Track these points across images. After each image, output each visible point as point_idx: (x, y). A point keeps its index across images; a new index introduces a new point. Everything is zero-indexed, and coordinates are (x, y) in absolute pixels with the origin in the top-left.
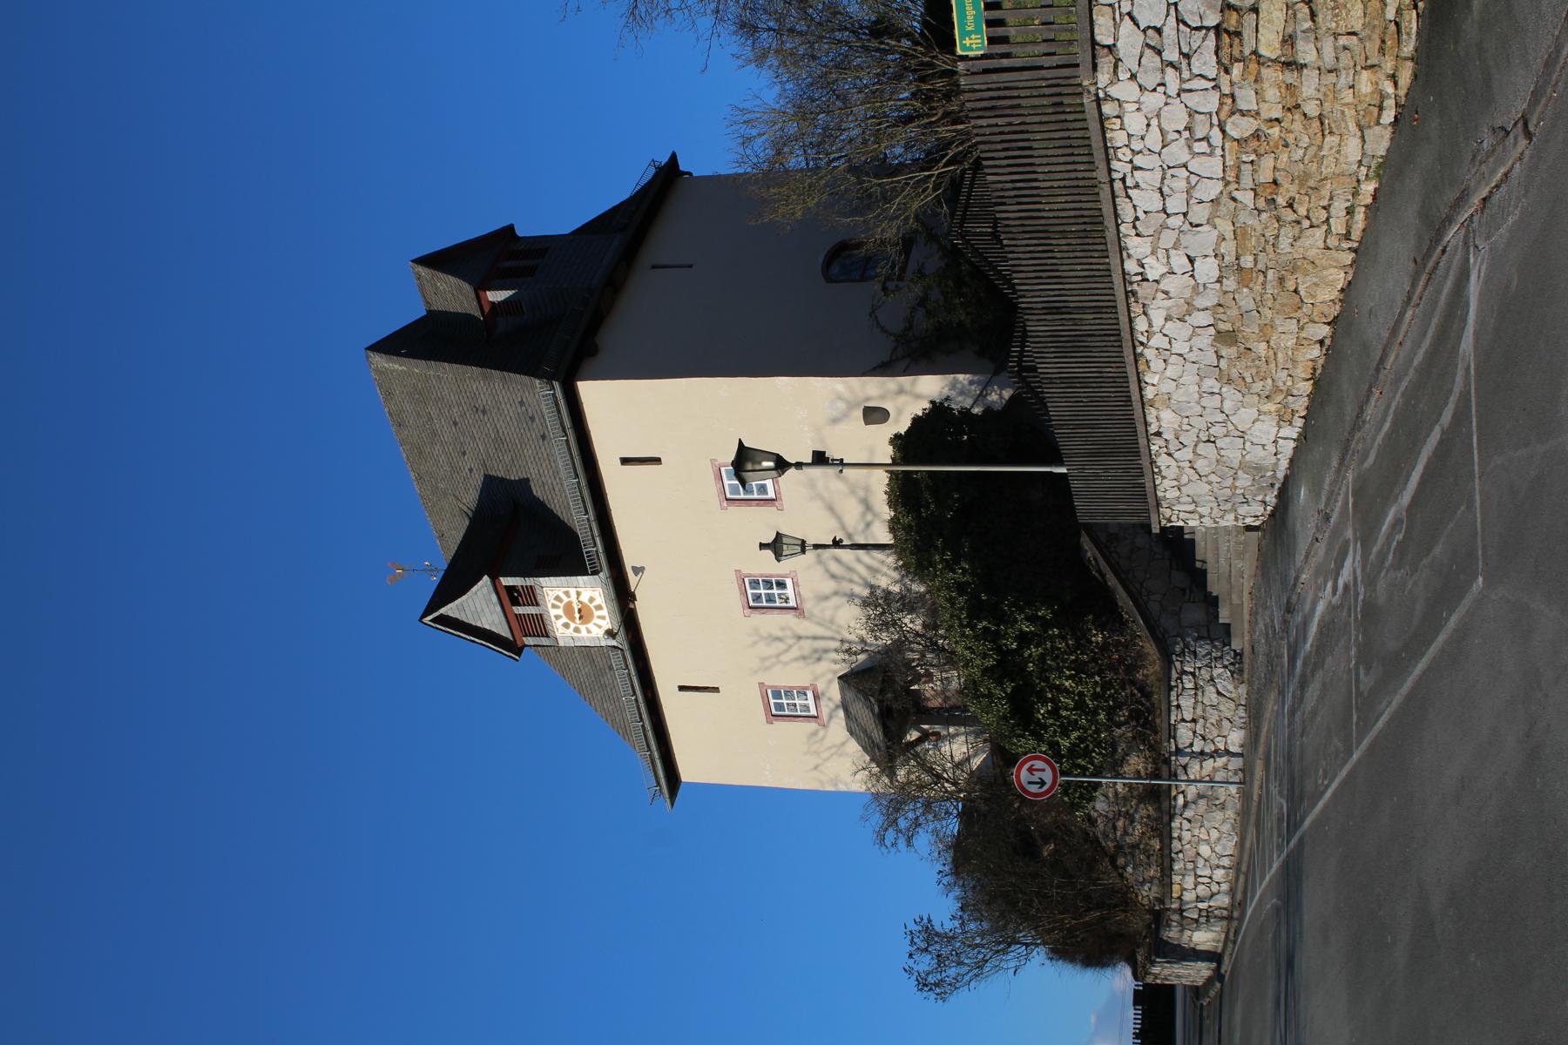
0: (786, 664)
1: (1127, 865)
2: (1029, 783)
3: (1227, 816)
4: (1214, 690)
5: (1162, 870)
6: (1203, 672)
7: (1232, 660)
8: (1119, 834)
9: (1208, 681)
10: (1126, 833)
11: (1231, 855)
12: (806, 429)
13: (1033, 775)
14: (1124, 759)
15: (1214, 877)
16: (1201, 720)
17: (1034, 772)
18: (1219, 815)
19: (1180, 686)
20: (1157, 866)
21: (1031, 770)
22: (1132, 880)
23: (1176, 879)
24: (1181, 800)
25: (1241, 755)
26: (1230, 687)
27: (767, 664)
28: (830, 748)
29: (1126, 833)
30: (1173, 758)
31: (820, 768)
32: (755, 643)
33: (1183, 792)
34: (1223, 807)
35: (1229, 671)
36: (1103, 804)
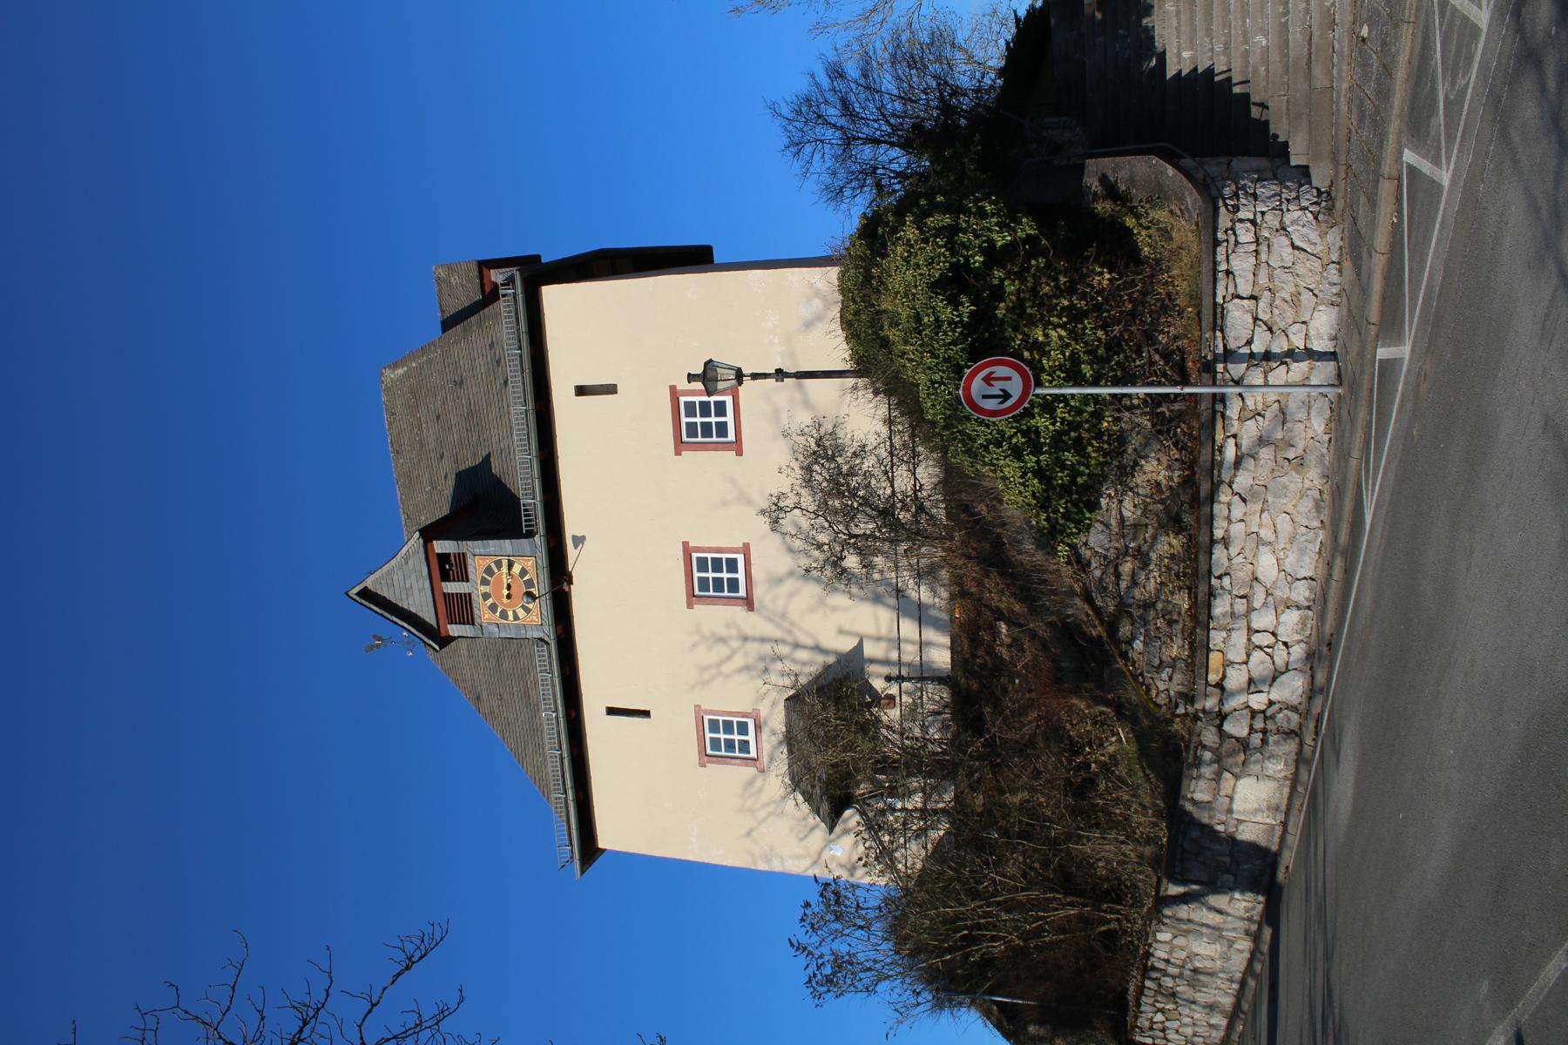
0: (727, 677)
1: (1134, 638)
2: (985, 397)
3: (1307, 484)
4: (1289, 243)
5: (1192, 648)
6: (1268, 217)
7: (1316, 199)
8: (1123, 585)
9: (1277, 231)
10: (1134, 583)
11: (1311, 578)
12: (776, 341)
13: (992, 385)
14: (1136, 464)
15: (1280, 631)
16: (1267, 293)
17: (1001, 393)
18: (1293, 480)
19: (1232, 239)
20: (1184, 639)
21: (988, 380)
22: (1141, 663)
23: (1217, 638)
24: (1230, 453)
25: (1333, 356)
26: (1314, 236)
27: (706, 676)
28: (768, 804)
29: (1134, 583)
30: (1220, 367)
31: (754, 834)
32: (695, 646)
33: (1235, 436)
34: (1300, 463)
35: (1311, 212)
36: (1101, 537)
